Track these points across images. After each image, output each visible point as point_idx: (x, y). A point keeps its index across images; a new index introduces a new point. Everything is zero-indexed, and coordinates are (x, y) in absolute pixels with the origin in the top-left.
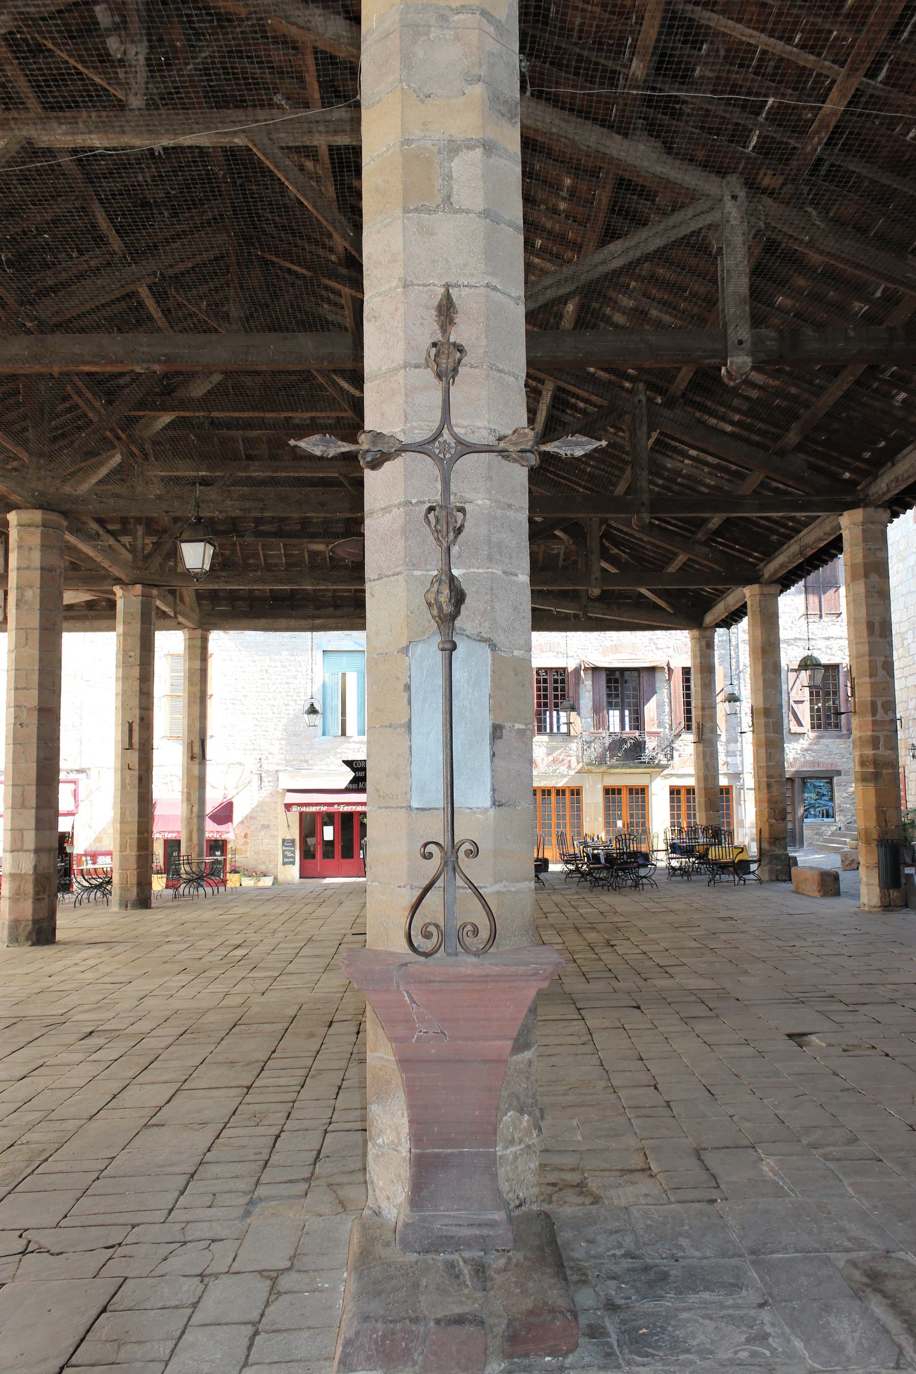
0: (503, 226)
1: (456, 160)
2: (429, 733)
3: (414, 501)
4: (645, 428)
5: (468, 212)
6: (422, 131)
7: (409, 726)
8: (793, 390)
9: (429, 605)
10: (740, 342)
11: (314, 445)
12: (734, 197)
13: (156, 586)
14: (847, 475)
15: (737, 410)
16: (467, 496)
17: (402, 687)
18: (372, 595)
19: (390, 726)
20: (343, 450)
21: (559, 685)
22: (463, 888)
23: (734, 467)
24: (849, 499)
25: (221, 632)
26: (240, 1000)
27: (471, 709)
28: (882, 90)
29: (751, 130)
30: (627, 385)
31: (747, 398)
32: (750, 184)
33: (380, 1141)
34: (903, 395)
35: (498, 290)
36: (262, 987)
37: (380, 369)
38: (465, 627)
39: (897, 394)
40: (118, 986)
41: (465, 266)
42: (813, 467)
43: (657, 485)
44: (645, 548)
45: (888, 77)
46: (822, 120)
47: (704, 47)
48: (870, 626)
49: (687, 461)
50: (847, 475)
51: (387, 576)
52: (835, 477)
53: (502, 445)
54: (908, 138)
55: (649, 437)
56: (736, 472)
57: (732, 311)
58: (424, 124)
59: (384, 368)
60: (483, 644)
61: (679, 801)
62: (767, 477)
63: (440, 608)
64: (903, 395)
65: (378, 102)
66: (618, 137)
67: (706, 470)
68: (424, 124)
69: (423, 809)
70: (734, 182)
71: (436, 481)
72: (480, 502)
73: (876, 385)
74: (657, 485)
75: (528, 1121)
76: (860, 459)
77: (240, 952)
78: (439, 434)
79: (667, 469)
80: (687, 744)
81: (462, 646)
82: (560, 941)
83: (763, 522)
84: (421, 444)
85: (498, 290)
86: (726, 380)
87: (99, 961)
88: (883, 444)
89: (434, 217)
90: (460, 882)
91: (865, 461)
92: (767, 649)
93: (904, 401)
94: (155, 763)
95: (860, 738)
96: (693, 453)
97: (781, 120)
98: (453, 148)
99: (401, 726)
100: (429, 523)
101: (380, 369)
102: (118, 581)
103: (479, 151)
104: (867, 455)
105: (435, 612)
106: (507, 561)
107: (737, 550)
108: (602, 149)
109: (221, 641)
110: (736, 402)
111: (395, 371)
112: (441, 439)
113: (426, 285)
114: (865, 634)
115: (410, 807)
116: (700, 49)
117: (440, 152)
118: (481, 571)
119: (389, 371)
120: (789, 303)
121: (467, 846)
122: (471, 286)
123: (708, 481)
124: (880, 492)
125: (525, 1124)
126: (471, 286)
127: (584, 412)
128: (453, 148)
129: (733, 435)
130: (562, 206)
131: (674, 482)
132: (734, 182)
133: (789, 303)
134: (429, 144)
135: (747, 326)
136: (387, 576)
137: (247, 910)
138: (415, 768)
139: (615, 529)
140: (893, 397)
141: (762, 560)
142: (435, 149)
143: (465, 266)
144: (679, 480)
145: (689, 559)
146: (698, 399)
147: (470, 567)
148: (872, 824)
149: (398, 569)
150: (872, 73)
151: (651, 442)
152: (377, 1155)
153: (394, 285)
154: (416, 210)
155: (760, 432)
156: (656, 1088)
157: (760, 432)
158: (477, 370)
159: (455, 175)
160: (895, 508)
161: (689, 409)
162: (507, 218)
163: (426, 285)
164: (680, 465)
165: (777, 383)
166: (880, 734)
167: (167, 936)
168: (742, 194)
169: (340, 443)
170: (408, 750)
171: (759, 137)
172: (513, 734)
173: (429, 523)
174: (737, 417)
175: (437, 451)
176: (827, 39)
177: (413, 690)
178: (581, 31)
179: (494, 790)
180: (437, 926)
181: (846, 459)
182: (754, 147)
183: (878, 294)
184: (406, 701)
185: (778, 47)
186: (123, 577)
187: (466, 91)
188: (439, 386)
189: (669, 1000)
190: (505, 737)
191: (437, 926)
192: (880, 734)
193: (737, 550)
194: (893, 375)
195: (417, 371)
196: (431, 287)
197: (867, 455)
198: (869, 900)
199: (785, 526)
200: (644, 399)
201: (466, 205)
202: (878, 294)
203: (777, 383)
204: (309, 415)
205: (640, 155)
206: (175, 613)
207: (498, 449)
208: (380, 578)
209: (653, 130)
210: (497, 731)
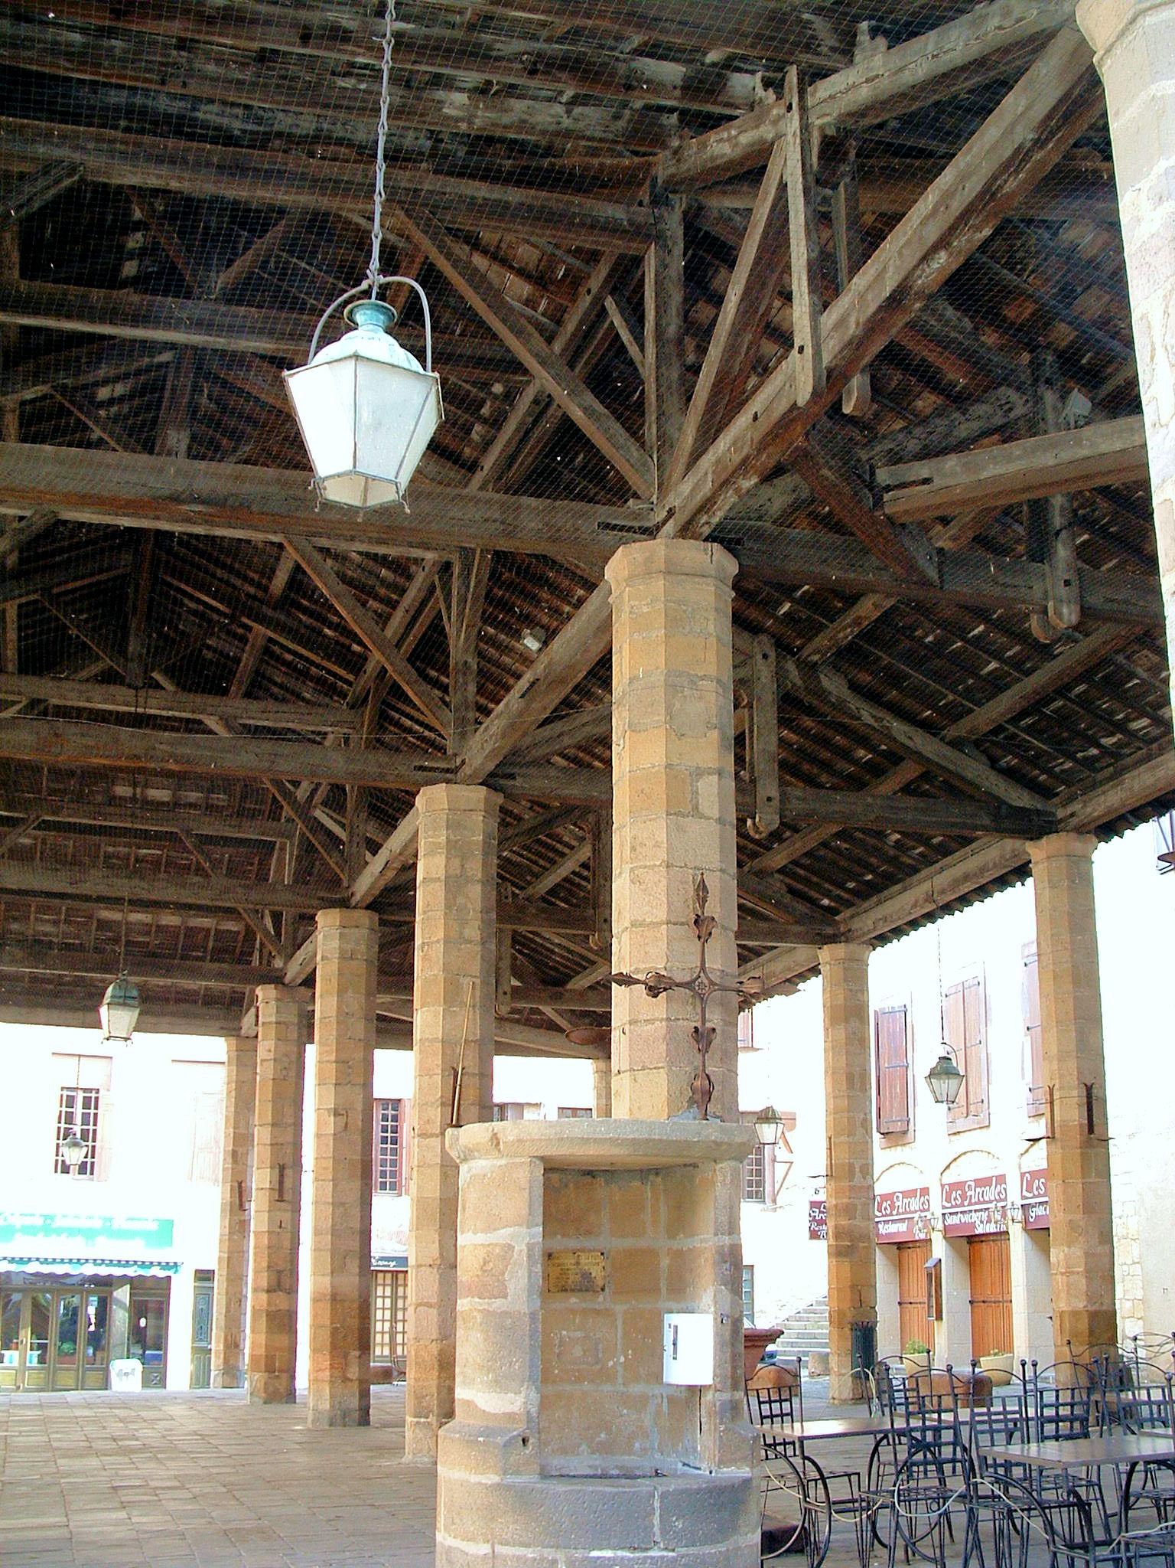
10: (769, 799)
12: (765, 657)
14: (826, 902)
21: (389, 1123)
24: (829, 931)
42: (791, 891)
44: (552, 952)
48: (850, 1078)
50: (826, 902)
52: (813, 902)
57: (762, 766)
59: (648, 920)
76: (842, 886)
84: (687, 983)
86: (752, 833)
91: (848, 891)
95: (836, 1206)
98: (699, 773)
103: (715, 778)
104: (851, 885)
111: (662, 924)
114: (844, 1087)
124: (866, 929)
128: (699, 773)
148: (846, 1305)
166: (857, 1202)
168: (772, 655)
181: (827, 885)
188: (699, 944)
192: (857, 1202)
197: (851, 885)
198: (840, 1393)
201: (707, 812)
208: (643, 1069)
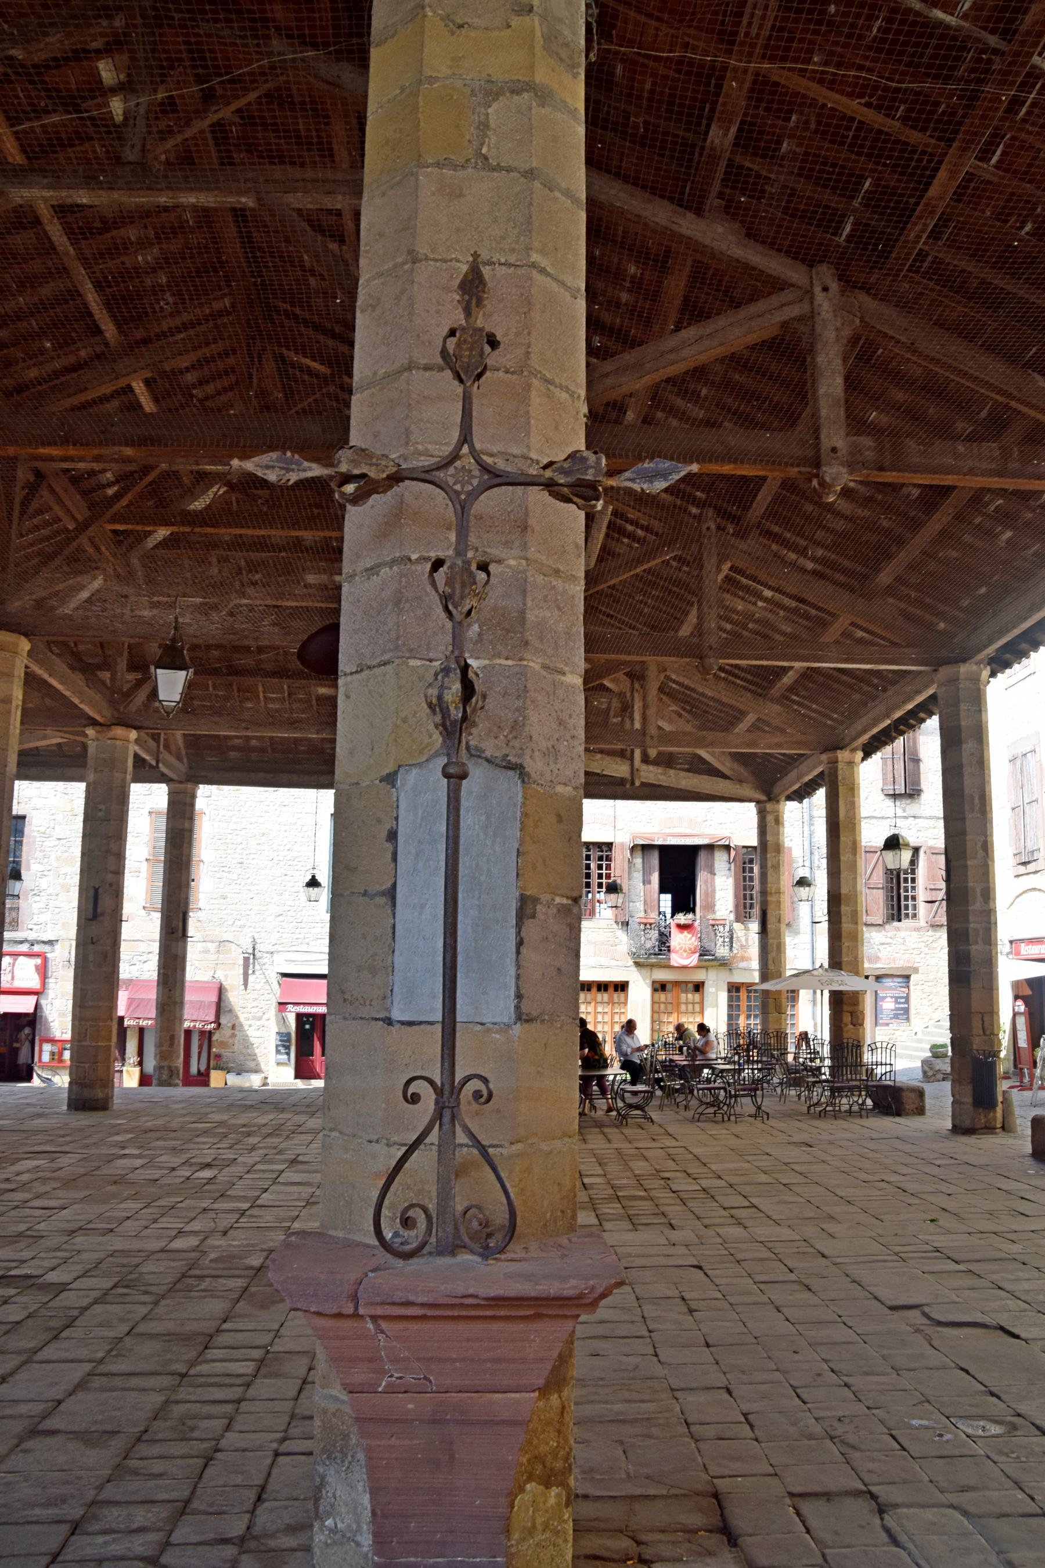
0: (557, 194)
1: (495, 106)
2: (422, 907)
3: (414, 557)
4: (714, 560)
5: (509, 170)
6: (451, 67)
7: (391, 894)
8: (885, 523)
9: (430, 705)
11: (267, 467)
12: (825, 289)
13: (135, 728)
14: (942, 625)
15: (819, 544)
16: (495, 552)
17: (384, 834)
18: (348, 697)
19: (365, 894)
20: (310, 474)
22: (467, 1146)
23: (814, 612)
25: (214, 788)
26: (193, 1241)
27: (489, 871)
28: (994, 174)
29: (844, 216)
30: (694, 510)
31: (833, 531)
32: (843, 277)
33: (329, 1522)
34: (1009, 534)
35: (549, 275)
36: (223, 1224)
37: (375, 374)
38: (482, 745)
39: (1002, 533)
40: (48, 1212)
41: (503, 238)
43: (725, 631)
45: (1000, 161)
46: (927, 205)
47: (794, 118)
49: (760, 604)
50: (942, 625)
51: (369, 667)
53: (548, 473)
54: (1023, 233)
55: (719, 570)
56: (817, 617)
58: (453, 59)
60: (511, 773)
61: (738, 999)
62: (853, 624)
63: (445, 713)
64: (1009, 534)
65: (392, 37)
66: (690, 215)
67: (782, 613)
68: (453, 59)
69: (410, 1024)
70: (825, 273)
71: (449, 528)
72: (512, 562)
73: (978, 520)
74: (725, 631)
75: (558, 1495)
77: (207, 1174)
78: (455, 457)
79: (737, 613)
80: (749, 935)
81: (478, 776)
82: (601, 1172)
83: (845, 678)
85: (549, 275)
87: (34, 1176)
88: (983, 590)
89: (461, 173)
90: (461, 1138)
92: (840, 828)
93: (1008, 541)
94: (123, 936)
96: (768, 593)
97: (865, 231)
99: (383, 894)
100: (434, 584)
101: (375, 374)
102: (94, 723)
105: (438, 719)
106: (550, 651)
107: (814, 711)
108: (675, 227)
109: (213, 801)
110: (820, 535)
112: (458, 464)
113: (445, 261)
115: (389, 1021)
116: (788, 120)
117: (473, 93)
118: (510, 663)
119: (387, 375)
120: (884, 419)
121: (475, 1085)
122: (510, 265)
123: (783, 627)
125: (552, 1501)
126: (510, 265)
127: (642, 541)
129: (815, 573)
130: (625, 297)
131: (745, 627)
132: (825, 273)
133: (884, 419)
134: (459, 83)
135: (842, 432)
136: (369, 667)
137: (225, 1117)
138: (399, 959)
139: (674, 681)
140: (997, 536)
141: (842, 723)
142: (468, 90)
143: (503, 238)
144: (750, 626)
145: (759, 719)
146: (776, 529)
147: (494, 656)
149: (386, 657)
150: (984, 155)
151: (721, 577)
152: (326, 1544)
153: (400, 260)
154: (438, 165)
155: (845, 571)
156: (729, 1392)
157: (845, 571)
158: (515, 377)
159: (492, 124)
160: (994, 666)
161: (765, 541)
162: (563, 185)
163: (445, 261)
164: (753, 608)
165: (866, 513)
167: (123, 1148)
168: (834, 286)
169: (306, 464)
170: (390, 931)
171: (854, 224)
172: (553, 911)
173: (434, 584)
174: (820, 552)
175: (451, 481)
176: (934, 112)
177: (401, 839)
178: (650, 100)
179: (519, 996)
180: (425, 1210)
182: (849, 236)
183: (983, 414)
184: (389, 856)
185: (877, 119)
186: (98, 718)
187: (513, 24)
189: (739, 1256)
190: (540, 915)
191: (425, 1210)
193: (814, 711)
194: (997, 509)
195: (427, 374)
196: (453, 263)
199: (869, 683)
200: (713, 526)
202: (983, 414)
203: (866, 513)
204: (322, 534)
205: (716, 235)
206: (157, 762)
207: (543, 480)
209: (730, 210)
210: (526, 908)
